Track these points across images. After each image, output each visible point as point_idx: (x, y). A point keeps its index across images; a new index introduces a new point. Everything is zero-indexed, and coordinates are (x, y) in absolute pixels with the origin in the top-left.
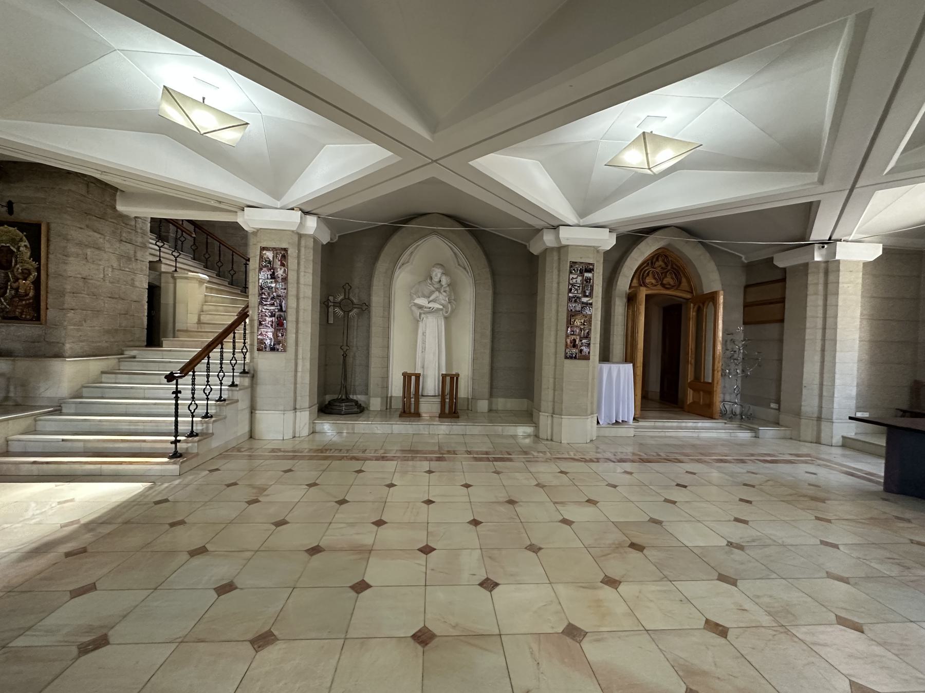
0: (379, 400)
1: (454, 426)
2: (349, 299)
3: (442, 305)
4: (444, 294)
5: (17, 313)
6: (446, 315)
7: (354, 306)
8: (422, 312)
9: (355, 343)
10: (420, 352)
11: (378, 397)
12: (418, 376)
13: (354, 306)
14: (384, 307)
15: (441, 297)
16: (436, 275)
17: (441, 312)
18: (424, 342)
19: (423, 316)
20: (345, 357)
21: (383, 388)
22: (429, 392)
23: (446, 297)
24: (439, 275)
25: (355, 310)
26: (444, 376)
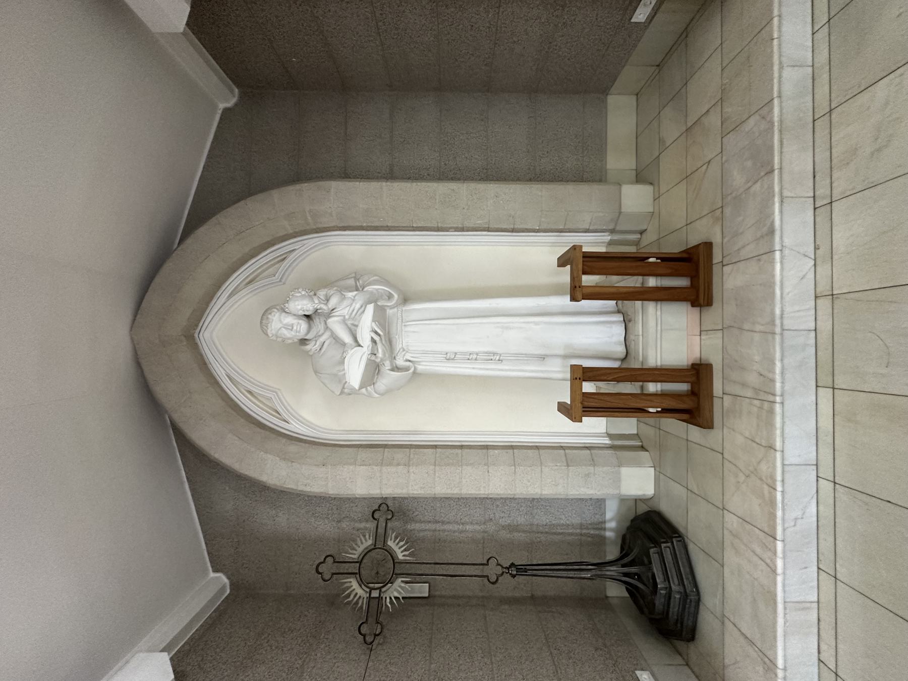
1: (787, 241)
4: (333, 301)
6: (396, 296)
9: (477, 527)
10: (500, 366)
11: (619, 473)
12: (582, 374)
14: (382, 465)
15: (344, 310)
16: (290, 327)
17: (390, 312)
18: (471, 357)
19: (400, 362)
20: (518, 570)
21: (593, 462)
22: (615, 339)
23: (343, 298)
24: (289, 320)
26: (577, 292)
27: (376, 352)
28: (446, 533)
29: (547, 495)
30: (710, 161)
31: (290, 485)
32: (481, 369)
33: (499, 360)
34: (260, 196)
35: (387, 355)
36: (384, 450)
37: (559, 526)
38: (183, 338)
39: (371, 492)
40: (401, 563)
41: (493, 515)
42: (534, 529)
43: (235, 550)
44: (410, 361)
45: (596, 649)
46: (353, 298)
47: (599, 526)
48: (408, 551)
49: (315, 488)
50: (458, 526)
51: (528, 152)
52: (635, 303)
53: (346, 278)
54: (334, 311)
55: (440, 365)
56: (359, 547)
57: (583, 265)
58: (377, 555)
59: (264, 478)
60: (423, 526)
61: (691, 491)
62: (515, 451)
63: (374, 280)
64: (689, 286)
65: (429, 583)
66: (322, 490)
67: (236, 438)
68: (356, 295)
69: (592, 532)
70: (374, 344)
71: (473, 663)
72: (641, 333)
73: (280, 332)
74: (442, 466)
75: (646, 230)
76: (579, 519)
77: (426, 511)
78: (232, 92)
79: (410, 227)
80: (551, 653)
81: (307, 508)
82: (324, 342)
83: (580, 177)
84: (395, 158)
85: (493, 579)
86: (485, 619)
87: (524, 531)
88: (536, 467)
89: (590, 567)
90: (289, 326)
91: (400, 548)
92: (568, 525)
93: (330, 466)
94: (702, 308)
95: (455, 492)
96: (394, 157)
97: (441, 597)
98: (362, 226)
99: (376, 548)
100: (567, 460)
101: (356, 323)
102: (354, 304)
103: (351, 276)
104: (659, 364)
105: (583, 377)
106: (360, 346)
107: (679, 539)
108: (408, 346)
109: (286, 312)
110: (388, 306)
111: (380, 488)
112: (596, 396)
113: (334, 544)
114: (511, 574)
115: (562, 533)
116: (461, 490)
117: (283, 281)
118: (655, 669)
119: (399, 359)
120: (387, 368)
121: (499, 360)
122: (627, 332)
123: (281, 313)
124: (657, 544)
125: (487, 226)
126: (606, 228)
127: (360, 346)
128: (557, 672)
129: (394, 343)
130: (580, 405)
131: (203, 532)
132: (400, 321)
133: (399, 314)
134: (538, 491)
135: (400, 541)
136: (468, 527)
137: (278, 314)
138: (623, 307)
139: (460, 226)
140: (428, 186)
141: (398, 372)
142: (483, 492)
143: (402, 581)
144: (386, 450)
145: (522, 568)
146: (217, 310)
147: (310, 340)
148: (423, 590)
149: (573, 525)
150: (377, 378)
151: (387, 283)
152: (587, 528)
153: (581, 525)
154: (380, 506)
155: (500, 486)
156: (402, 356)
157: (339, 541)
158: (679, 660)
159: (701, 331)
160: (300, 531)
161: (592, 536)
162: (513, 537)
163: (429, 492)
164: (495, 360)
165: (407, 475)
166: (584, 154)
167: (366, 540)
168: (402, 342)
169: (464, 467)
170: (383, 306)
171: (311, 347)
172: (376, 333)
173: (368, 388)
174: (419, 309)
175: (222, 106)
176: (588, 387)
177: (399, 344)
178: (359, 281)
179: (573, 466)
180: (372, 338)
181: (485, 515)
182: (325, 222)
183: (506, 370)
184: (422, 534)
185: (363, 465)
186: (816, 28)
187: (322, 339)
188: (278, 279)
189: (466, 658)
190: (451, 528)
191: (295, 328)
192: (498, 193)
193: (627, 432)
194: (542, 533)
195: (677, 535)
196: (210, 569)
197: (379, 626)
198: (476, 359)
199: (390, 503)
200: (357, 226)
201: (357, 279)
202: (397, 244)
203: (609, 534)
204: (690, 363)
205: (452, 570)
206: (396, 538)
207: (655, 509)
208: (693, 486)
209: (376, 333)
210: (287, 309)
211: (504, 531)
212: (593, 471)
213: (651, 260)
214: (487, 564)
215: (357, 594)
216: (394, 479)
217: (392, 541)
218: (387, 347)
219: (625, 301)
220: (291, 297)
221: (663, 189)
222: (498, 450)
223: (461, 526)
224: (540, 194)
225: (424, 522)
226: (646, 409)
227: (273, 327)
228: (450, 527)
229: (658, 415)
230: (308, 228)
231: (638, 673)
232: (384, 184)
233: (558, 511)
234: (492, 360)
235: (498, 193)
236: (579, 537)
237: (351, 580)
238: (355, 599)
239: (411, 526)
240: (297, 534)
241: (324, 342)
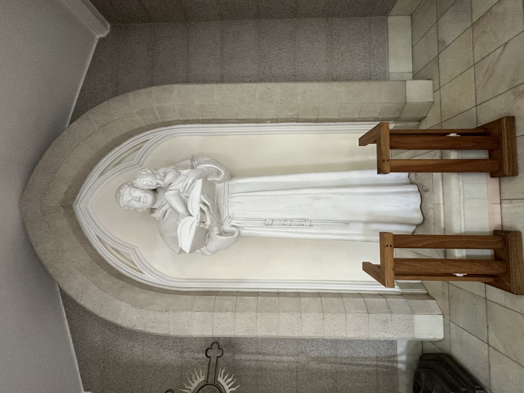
0: (418, 318)
3: (474, 23)
4: (169, 178)
5: (226, 354)
8: (216, 230)
14: (213, 311)
17: (218, 186)
18: (286, 223)
19: (227, 227)
24: (138, 193)
25: (220, 379)
27: (205, 221)
28: (266, 363)
30: (506, 43)
31: (140, 328)
32: (294, 232)
33: (310, 225)
34: (121, 97)
35: (215, 222)
36: (216, 298)
37: (359, 358)
38: (61, 207)
41: (304, 348)
42: (339, 361)
43: (101, 373)
44: (235, 226)
46: (187, 174)
47: (392, 359)
49: (160, 330)
50: (276, 357)
51: (327, 62)
52: (432, 175)
53: (186, 159)
54: (171, 186)
55: (261, 229)
56: (194, 383)
57: (390, 140)
59: (119, 322)
60: (248, 357)
61: (494, 348)
62: (322, 299)
63: (206, 161)
64: (487, 158)
67: (98, 289)
68: (190, 172)
69: (386, 364)
70: (203, 214)
72: (442, 202)
73: (130, 203)
74: (263, 312)
75: (426, 117)
76: (375, 353)
77: (250, 345)
78: (106, 26)
79: (236, 119)
81: (157, 340)
82: (166, 211)
83: (368, 78)
84: (225, 70)
87: (331, 363)
88: (341, 314)
90: (137, 198)
91: (228, 385)
92: (366, 358)
93: (171, 312)
94: (501, 178)
95: (274, 335)
96: (224, 69)
98: (198, 120)
99: (207, 385)
100: (367, 307)
101: (188, 196)
102: (187, 180)
103: (188, 158)
104: (463, 230)
105: (394, 244)
106: (191, 215)
108: (233, 214)
109: (135, 187)
110: (217, 181)
111: (212, 330)
112: (406, 263)
113: (178, 370)
115: (361, 365)
117: (141, 163)
119: (226, 225)
120: (215, 233)
121: (310, 225)
122: (424, 201)
123: (131, 189)
125: (296, 117)
126: (393, 117)
127: (191, 215)
129: (221, 211)
130: (392, 271)
131: (78, 359)
132: (227, 193)
133: (226, 188)
135: (229, 377)
136: (284, 358)
137: (128, 189)
138: (416, 179)
139: (275, 117)
140: (250, 86)
141: (226, 236)
142: (297, 334)
144: (217, 297)
146: (89, 186)
147: (157, 209)
149: (370, 358)
150: (208, 241)
151: (217, 162)
152: (381, 361)
155: (311, 329)
156: (228, 223)
157: (182, 367)
159: (501, 200)
160: (151, 359)
161: (387, 367)
162: (321, 367)
164: (307, 225)
165: (234, 320)
166: (371, 62)
167: (200, 377)
168: (228, 210)
169: (281, 314)
170: (213, 181)
171: (158, 214)
172: (205, 204)
173: (202, 248)
174: (242, 184)
175: (98, 36)
176: (400, 253)
177: (226, 212)
178: (195, 162)
180: (201, 208)
182: (170, 117)
183: (316, 234)
184: (247, 363)
185: (198, 311)
186: (440, 51)
187: (164, 209)
188: (136, 162)
190: (270, 359)
191: (142, 200)
192: (305, 90)
194: (345, 364)
196: (82, 389)
198: (290, 225)
199: (221, 343)
200: (194, 120)
201: (192, 160)
202: (226, 134)
203: (401, 366)
204: (492, 230)
206: (225, 374)
207: (446, 352)
208: (494, 340)
209: (205, 204)
210: (135, 185)
211: (314, 362)
212: (390, 317)
213: (452, 135)
217: (222, 377)
218: (215, 215)
219: (418, 173)
220: (138, 175)
221: (444, 79)
222: (309, 298)
223: (279, 357)
224: (339, 90)
225: (249, 353)
226: (453, 274)
227: (124, 200)
229: (464, 279)
230: (157, 122)
232: (215, 85)
234: (303, 225)
235: (305, 90)
236: (376, 368)
239: (237, 357)
241: (166, 211)
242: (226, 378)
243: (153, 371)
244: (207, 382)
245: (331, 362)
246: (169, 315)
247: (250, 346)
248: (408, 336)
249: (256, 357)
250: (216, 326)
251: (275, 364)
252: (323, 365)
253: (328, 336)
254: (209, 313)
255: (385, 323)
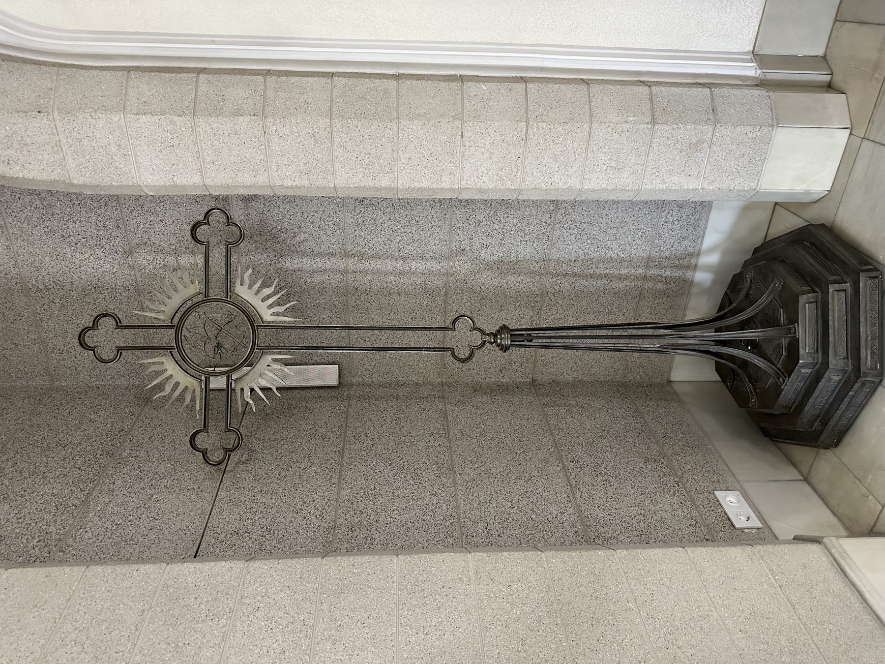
2: (177, 325)
7: (216, 292)
9: (434, 266)
13: (216, 292)
21: (714, 116)
25: (243, 292)
29: (593, 191)
36: (197, 78)
39: (179, 181)
40: (269, 326)
41: (467, 241)
45: (647, 461)
48: (281, 305)
50: (394, 263)
58: (218, 313)
60: (319, 263)
65: (339, 365)
66: (54, 176)
71: (421, 486)
77: (322, 233)
80: (564, 466)
85: (464, 353)
86: (446, 417)
89: (662, 331)
92: (622, 260)
95: (384, 184)
97: (362, 385)
99: (209, 301)
107: (874, 274)
111: (200, 171)
114: (498, 345)
115: (606, 276)
116: (397, 178)
118: (747, 486)
124: (816, 284)
128: (574, 494)
134: (574, 182)
135: (265, 285)
136: (414, 265)
143: (274, 360)
145: (523, 335)
148: (329, 375)
153: (649, 259)
154: (207, 215)
158: (792, 473)
161: (667, 281)
163: (321, 183)
179: (665, 123)
181: (450, 241)
184: (318, 278)
189: (407, 478)
193: (801, 52)
195: (871, 267)
197: (233, 436)
199: (238, 214)
205: (383, 339)
214: (454, 329)
215: (177, 384)
216: (230, 149)
228: (377, 265)
231: (719, 494)
233: (605, 233)
237: (163, 359)
238: (177, 393)
240: (40, 278)
242: (256, 287)
243: (57, 301)
244: (206, 295)
245: (534, 272)
246: (52, 125)
247: (324, 238)
248: (741, 184)
249: (341, 264)
250: (209, 159)
251: (392, 278)
252: (512, 279)
253: (533, 186)
254: (181, 119)
255: (694, 150)
